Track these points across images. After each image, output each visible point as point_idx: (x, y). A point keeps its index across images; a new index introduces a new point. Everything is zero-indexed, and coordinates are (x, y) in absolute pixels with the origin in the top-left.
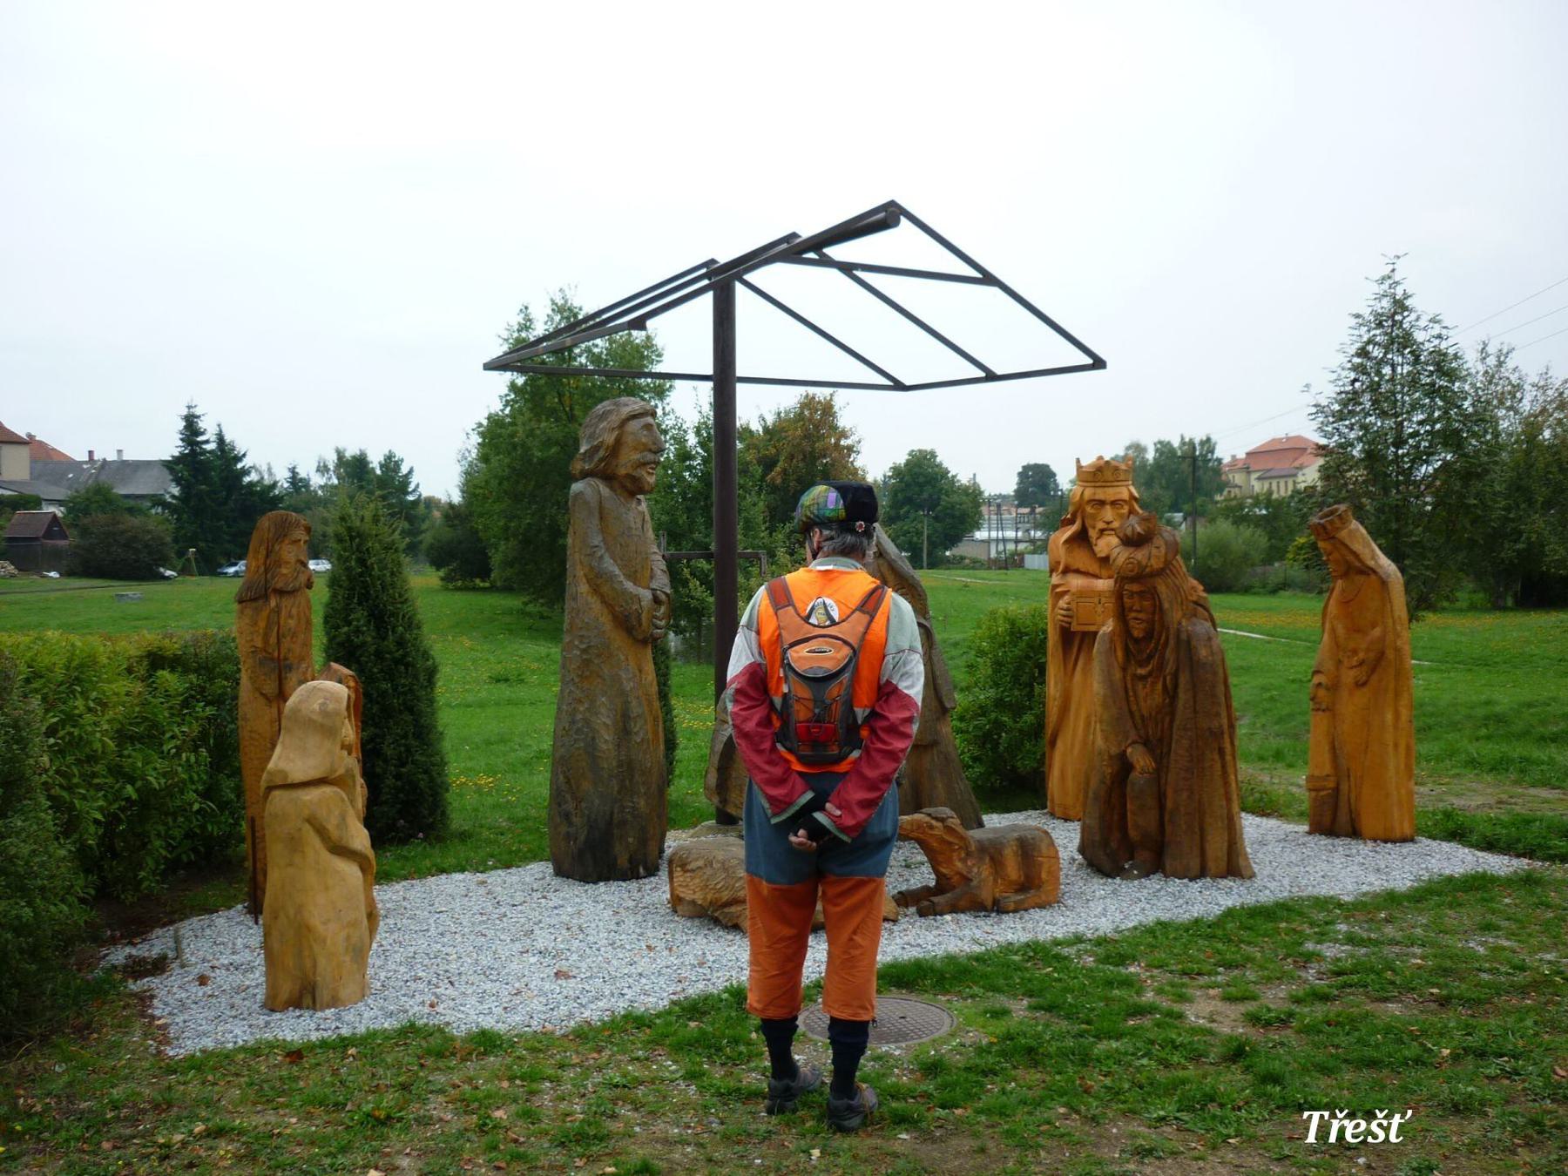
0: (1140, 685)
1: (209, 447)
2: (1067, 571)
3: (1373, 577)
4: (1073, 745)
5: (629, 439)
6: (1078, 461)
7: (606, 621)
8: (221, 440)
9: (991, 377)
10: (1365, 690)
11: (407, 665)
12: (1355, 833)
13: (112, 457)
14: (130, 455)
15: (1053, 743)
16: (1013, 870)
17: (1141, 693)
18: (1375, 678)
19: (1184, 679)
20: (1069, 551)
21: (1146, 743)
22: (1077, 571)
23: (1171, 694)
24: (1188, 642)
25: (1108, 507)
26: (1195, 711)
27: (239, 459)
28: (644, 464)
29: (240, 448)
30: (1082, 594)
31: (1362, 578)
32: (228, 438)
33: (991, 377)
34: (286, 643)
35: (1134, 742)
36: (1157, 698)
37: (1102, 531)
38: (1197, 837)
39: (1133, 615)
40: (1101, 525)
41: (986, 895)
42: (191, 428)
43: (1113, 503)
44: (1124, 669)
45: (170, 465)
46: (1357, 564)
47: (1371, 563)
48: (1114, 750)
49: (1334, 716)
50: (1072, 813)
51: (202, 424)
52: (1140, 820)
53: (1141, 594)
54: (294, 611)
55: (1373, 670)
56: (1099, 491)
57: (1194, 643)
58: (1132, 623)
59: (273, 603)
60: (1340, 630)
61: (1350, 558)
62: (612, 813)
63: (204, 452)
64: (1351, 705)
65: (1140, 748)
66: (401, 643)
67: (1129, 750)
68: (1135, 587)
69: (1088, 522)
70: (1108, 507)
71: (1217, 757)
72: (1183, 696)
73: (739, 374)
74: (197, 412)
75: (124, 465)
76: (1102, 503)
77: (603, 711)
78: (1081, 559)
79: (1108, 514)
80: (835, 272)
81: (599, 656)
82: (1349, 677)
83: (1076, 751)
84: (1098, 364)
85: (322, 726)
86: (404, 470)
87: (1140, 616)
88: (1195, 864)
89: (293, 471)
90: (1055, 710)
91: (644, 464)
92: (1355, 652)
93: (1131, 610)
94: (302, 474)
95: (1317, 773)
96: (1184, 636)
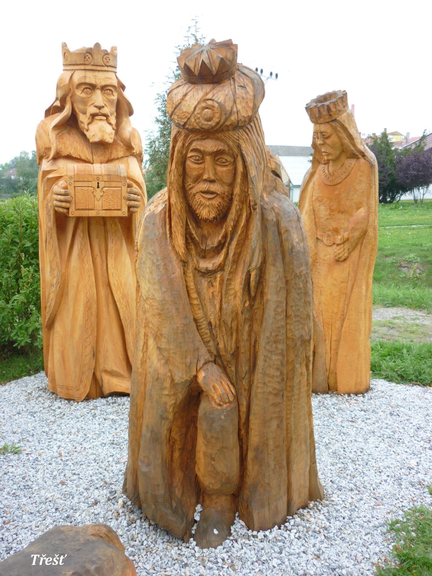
0: (204, 283)
2: (57, 157)
3: (362, 160)
4: (73, 331)
6: (64, 45)
10: (346, 265)
15: (50, 326)
17: (207, 293)
19: (273, 276)
20: (59, 137)
21: (217, 359)
22: (69, 157)
23: (254, 291)
24: (278, 224)
25: (98, 92)
26: (287, 316)
30: (78, 178)
36: (236, 299)
37: (93, 116)
39: (203, 186)
40: (92, 110)
43: (103, 88)
44: (185, 263)
48: (181, 376)
50: (75, 394)
52: (214, 462)
53: (217, 155)
56: (89, 74)
58: (199, 198)
60: (323, 212)
61: (347, 141)
65: (214, 369)
67: (202, 375)
68: (210, 145)
69: (78, 107)
70: (98, 92)
72: (272, 295)
76: (92, 87)
78: (72, 144)
83: (77, 334)
85: (232, 194)
87: (214, 187)
90: (52, 296)
92: (336, 231)
93: (198, 179)
96: (271, 216)
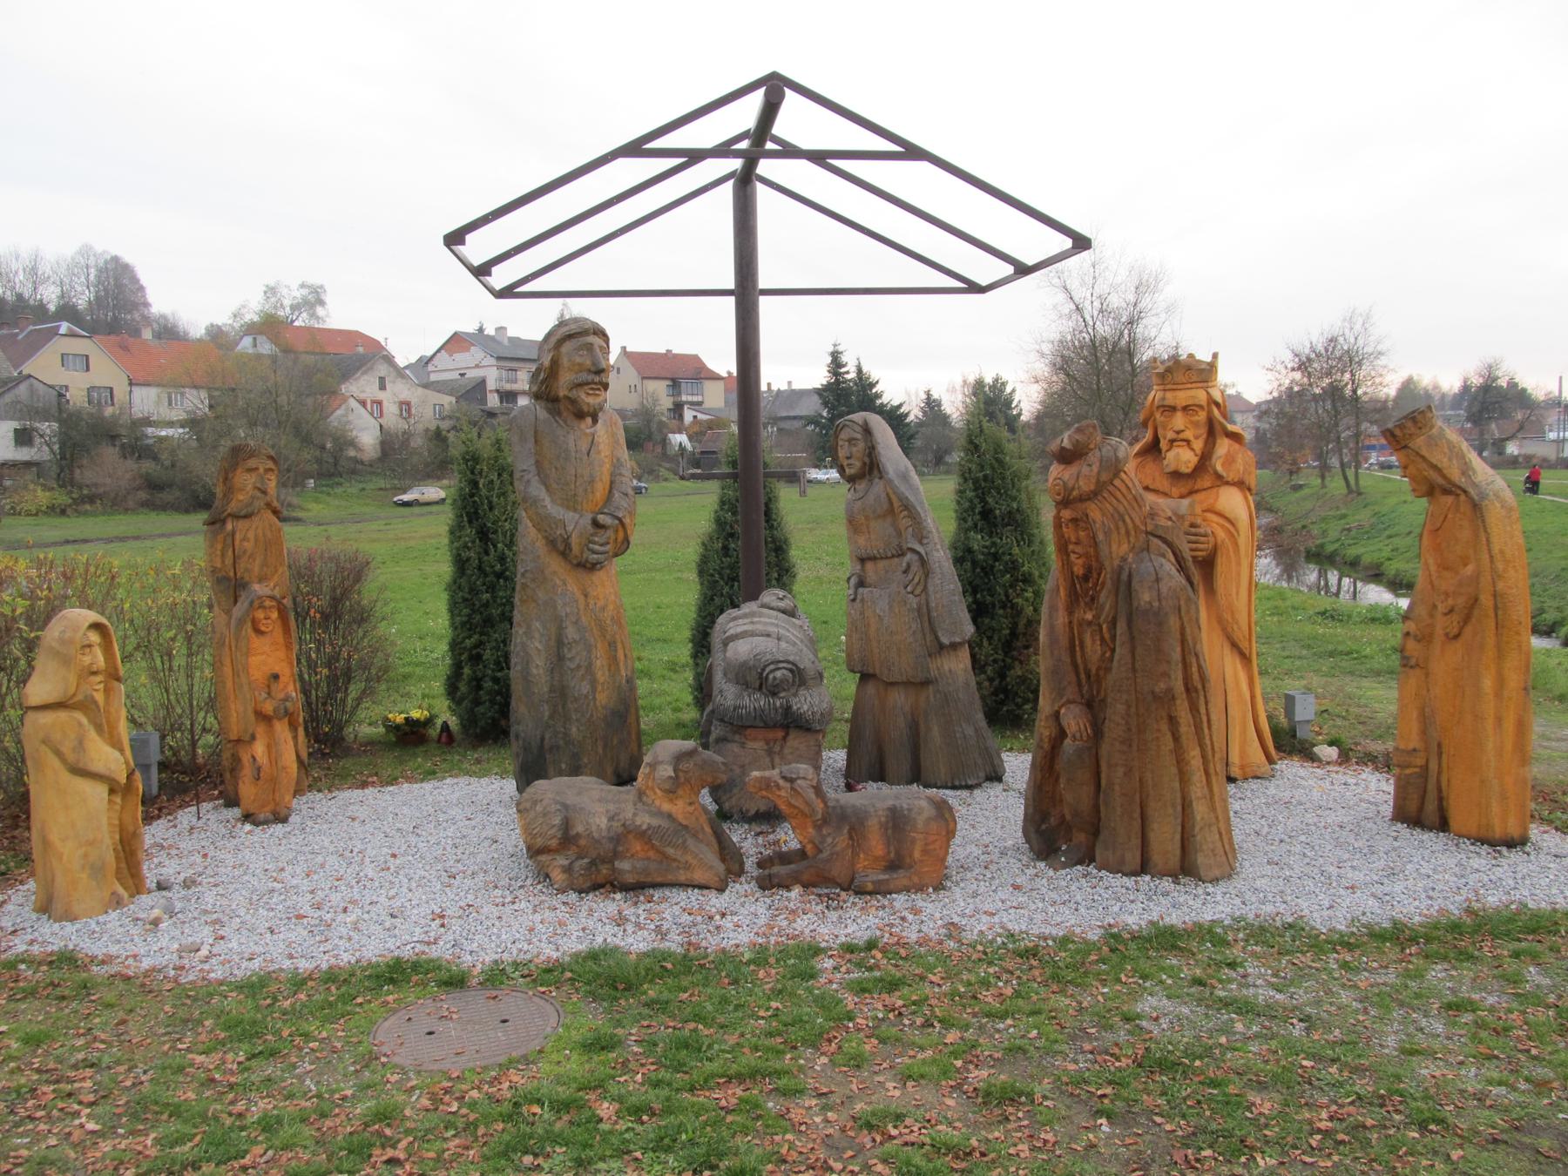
1: (848, 377)
5: (565, 361)
7: (540, 544)
8: (860, 371)
9: (1022, 270)
11: (506, 579)
12: (1443, 825)
13: (784, 387)
14: (795, 386)
16: (876, 844)
18: (1468, 630)
25: (1179, 414)
26: (1134, 670)
27: (872, 385)
28: (580, 385)
29: (874, 377)
31: (1450, 499)
32: (865, 370)
33: (1022, 270)
34: (242, 566)
35: (1069, 702)
37: (1172, 441)
38: (1137, 824)
40: (1171, 435)
41: (838, 870)
42: (836, 363)
44: (1070, 613)
45: (819, 392)
46: (1440, 480)
47: (1455, 474)
49: (1427, 675)
51: (844, 359)
52: (1074, 795)
54: (251, 535)
55: (1467, 619)
56: (1169, 395)
57: (1135, 584)
59: (229, 526)
62: (543, 739)
63: (846, 381)
64: (1445, 660)
65: (1076, 709)
66: (502, 559)
70: (1179, 414)
71: (1164, 727)
73: (762, 285)
74: (840, 349)
75: (793, 392)
76: (1173, 409)
77: (537, 635)
79: (1179, 421)
80: (804, 163)
81: (533, 580)
82: (1441, 625)
84: (1081, 243)
86: (1008, 390)
88: (1133, 858)
89: (928, 393)
91: (580, 385)
94: (935, 396)
95: (1402, 747)
